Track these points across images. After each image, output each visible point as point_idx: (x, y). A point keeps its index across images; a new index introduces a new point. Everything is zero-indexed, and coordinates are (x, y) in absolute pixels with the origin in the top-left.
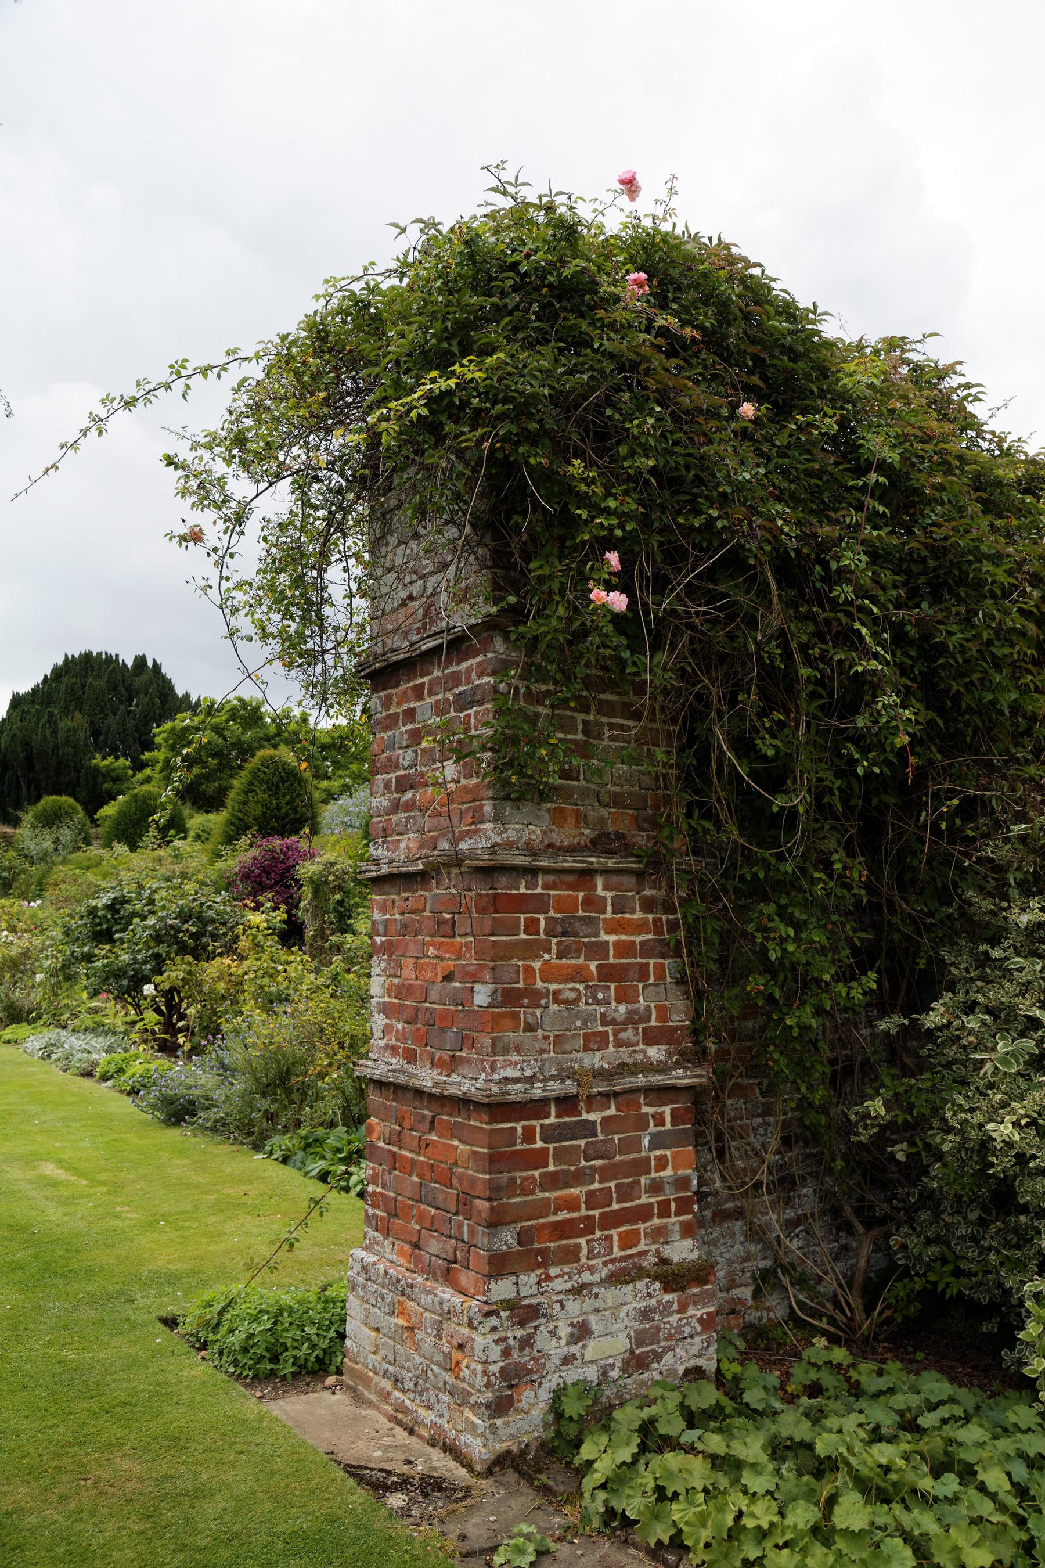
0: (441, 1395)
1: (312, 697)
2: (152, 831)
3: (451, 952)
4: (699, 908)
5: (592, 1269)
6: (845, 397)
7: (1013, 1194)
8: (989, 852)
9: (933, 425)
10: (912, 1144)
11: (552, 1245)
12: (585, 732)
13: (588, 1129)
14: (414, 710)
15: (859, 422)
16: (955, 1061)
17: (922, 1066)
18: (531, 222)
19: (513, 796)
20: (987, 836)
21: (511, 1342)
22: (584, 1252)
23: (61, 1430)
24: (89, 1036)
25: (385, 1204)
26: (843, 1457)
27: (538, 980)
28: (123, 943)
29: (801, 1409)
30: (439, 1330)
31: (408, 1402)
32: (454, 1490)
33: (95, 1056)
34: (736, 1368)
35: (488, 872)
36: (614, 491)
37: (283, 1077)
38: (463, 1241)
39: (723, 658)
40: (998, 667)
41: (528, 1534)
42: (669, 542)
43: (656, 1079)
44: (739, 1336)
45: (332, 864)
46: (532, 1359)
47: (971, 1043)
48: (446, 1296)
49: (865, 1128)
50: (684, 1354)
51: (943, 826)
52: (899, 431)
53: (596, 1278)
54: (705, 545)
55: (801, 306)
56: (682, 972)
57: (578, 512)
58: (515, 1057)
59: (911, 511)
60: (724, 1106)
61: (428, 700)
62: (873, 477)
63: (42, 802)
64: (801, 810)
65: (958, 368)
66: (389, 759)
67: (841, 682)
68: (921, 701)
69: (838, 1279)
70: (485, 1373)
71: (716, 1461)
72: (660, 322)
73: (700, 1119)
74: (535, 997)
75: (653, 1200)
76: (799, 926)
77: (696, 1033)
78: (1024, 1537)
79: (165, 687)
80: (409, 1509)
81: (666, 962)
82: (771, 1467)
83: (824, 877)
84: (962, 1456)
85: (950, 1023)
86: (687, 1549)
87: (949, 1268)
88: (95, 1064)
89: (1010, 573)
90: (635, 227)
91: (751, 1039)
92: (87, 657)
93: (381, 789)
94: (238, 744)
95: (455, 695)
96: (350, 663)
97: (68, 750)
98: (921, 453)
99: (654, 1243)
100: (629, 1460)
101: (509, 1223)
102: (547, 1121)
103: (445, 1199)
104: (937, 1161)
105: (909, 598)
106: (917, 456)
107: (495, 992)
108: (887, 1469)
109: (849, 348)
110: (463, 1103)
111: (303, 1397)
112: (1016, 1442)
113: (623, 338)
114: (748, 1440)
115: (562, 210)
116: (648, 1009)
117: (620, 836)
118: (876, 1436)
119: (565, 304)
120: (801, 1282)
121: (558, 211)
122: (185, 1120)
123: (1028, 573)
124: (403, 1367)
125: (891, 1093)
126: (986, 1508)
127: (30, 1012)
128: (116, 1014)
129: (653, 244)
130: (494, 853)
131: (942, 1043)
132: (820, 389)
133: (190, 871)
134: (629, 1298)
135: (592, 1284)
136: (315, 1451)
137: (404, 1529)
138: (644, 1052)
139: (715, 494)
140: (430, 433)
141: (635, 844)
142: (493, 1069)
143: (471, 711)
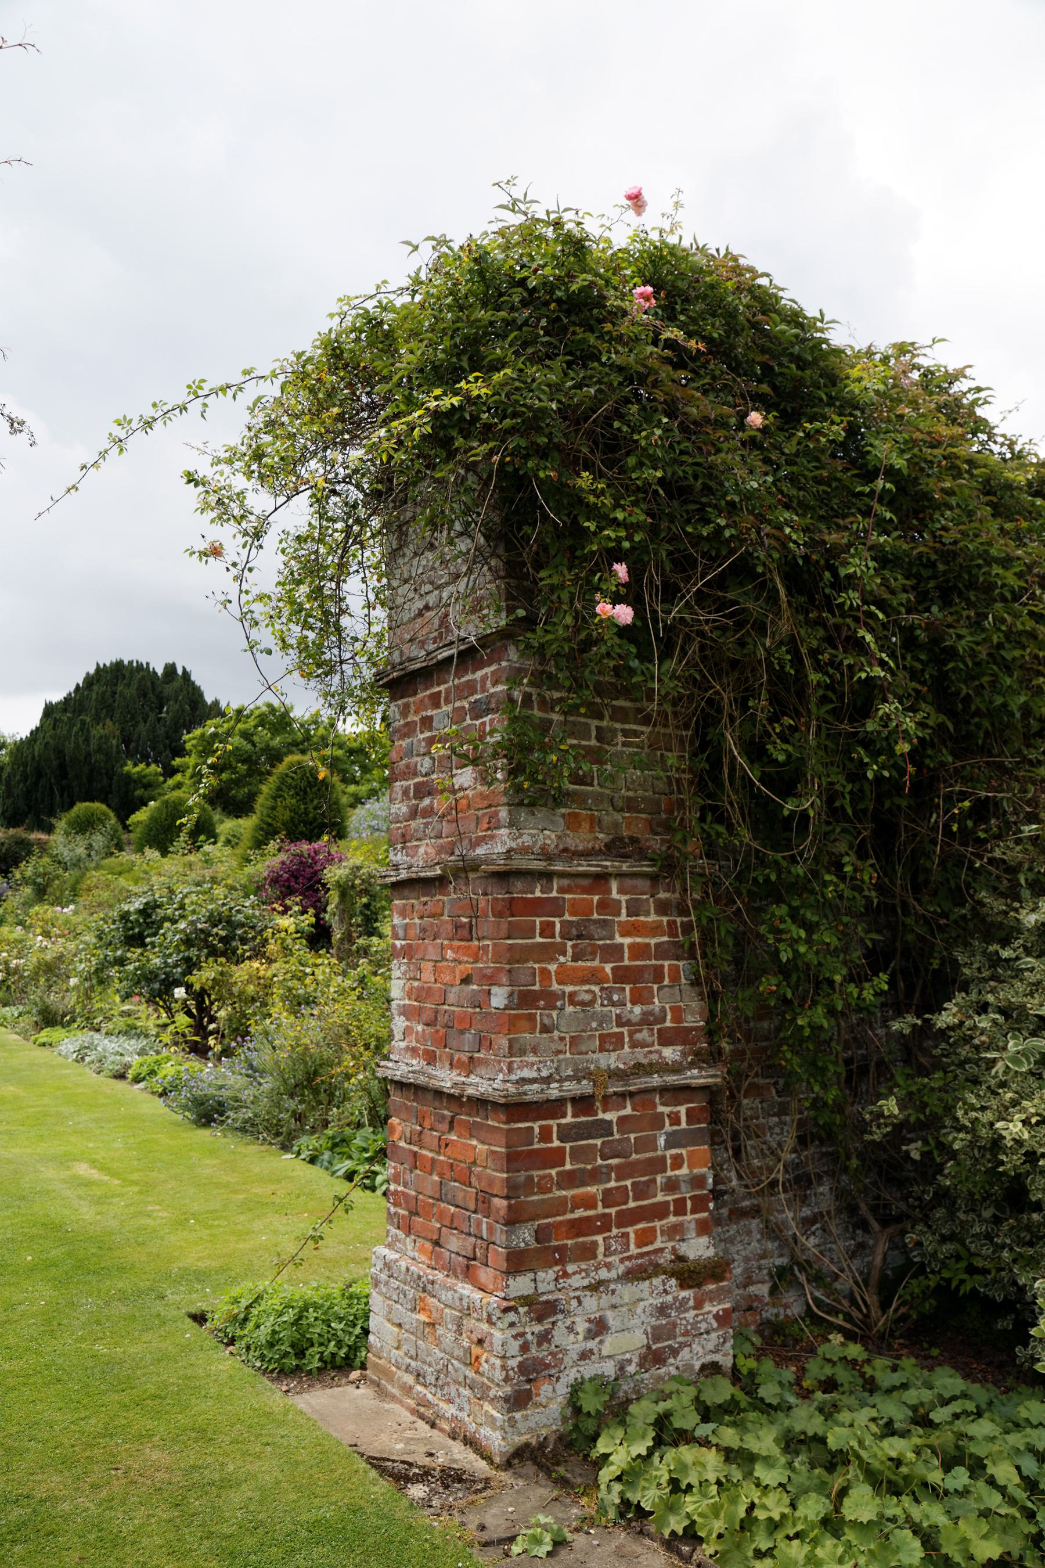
0: (461, 1389)
1: (330, 705)
2: (183, 836)
3: (469, 956)
4: (713, 910)
5: (609, 1266)
6: (852, 404)
7: (1026, 1192)
8: (997, 854)
9: (945, 431)
10: (926, 1142)
11: (569, 1242)
12: (599, 738)
13: (605, 1128)
14: (431, 718)
15: (868, 428)
16: (967, 1061)
17: (937, 1065)
18: (540, 238)
19: (526, 801)
20: (999, 837)
21: (529, 1337)
22: (601, 1249)
23: (93, 1421)
24: (122, 1039)
25: (407, 1202)
26: (854, 1451)
27: (554, 982)
28: (154, 947)
29: (816, 1403)
30: (459, 1326)
31: (429, 1396)
32: (474, 1482)
33: (128, 1059)
34: (752, 1363)
35: (504, 876)
36: (622, 502)
37: (311, 1076)
38: (482, 1238)
39: (734, 664)
40: (1008, 669)
41: (546, 1524)
42: (680, 551)
43: (671, 1079)
44: (755, 1332)
45: (359, 868)
46: (550, 1354)
47: (983, 1043)
48: (466, 1292)
49: (879, 1127)
50: (700, 1350)
51: (955, 828)
52: (907, 437)
53: (613, 1274)
54: (713, 553)
55: (809, 314)
56: (696, 973)
57: (586, 524)
58: (531, 1058)
59: (921, 516)
60: (740, 1105)
61: (445, 708)
62: (880, 483)
63: (76, 809)
64: (811, 813)
65: (968, 372)
66: (408, 766)
67: (851, 686)
68: (932, 704)
69: (854, 1277)
70: (504, 1367)
71: (730, 1455)
72: (666, 335)
73: (715, 1117)
74: (551, 999)
75: (669, 1198)
76: (810, 928)
77: (711, 1033)
78: (1033, 1530)
79: (194, 694)
80: (430, 1500)
81: (681, 964)
82: (783, 1460)
83: (835, 880)
84: (972, 1450)
85: (962, 1023)
86: (700, 1540)
87: (963, 1264)
88: (127, 1066)
89: (1020, 575)
90: (642, 242)
91: (767, 1039)
92: (118, 665)
93: (400, 796)
94: (267, 749)
95: (470, 703)
96: (368, 673)
97: (100, 757)
98: (930, 458)
99: (670, 1240)
100: (644, 1453)
101: (527, 1221)
102: (563, 1121)
103: (465, 1197)
104: (950, 1159)
105: (919, 603)
106: (926, 461)
107: (511, 995)
108: (898, 1462)
109: (858, 355)
110: (480, 1103)
111: (328, 1391)
112: (1026, 1436)
113: (631, 351)
114: (761, 1433)
115: (570, 226)
116: (663, 1010)
117: (634, 840)
118: (889, 1430)
119: (573, 318)
120: (817, 1279)
121: (566, 227)
122: (214, 1121)
123: (1038, 576)
124: (424, 1362)
125: (904, 1092)
126: (994, 1500)
127: (64, 1016)
128: (148, 1017)
129: (662, 257)
130: (509, 858)
131: (955, 1042)
132: (830, 397)
133: (220, 876)
134: (646, 1295)
135: (609, 1281)
136: (339, 1443)
137: (424, 1518)
138: (659, 1052)
139: (723, 503)
140: (442, 447)
141: (649, 848)
142: (510, 1070)
143: (487, 719)
